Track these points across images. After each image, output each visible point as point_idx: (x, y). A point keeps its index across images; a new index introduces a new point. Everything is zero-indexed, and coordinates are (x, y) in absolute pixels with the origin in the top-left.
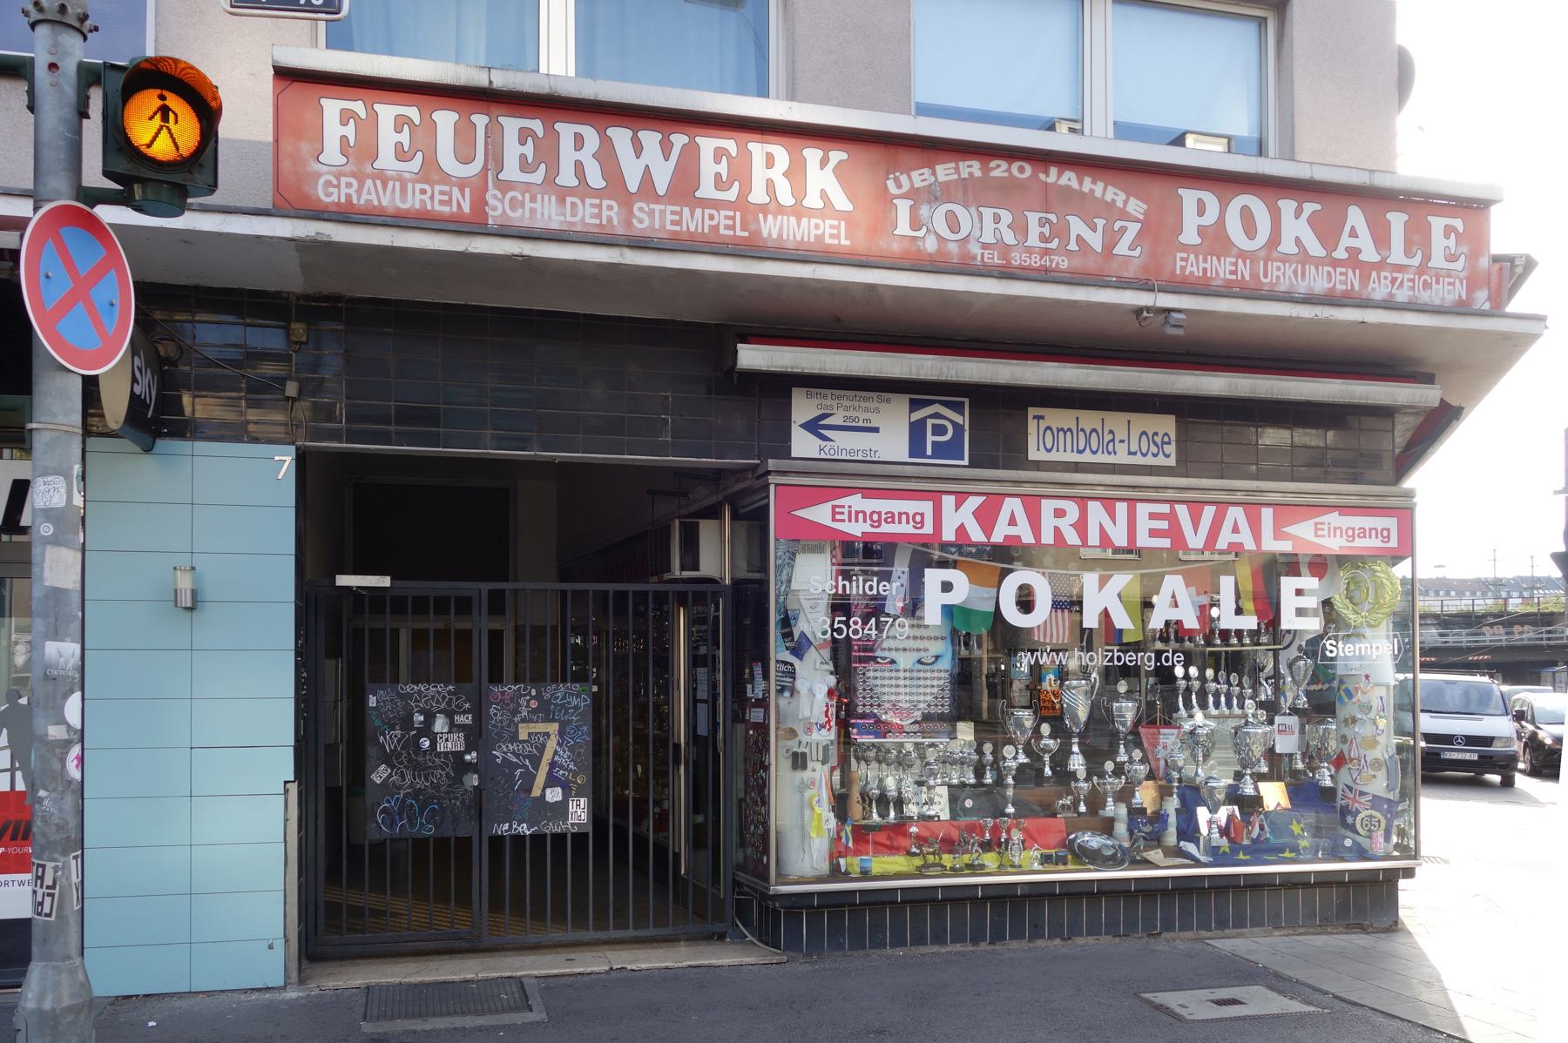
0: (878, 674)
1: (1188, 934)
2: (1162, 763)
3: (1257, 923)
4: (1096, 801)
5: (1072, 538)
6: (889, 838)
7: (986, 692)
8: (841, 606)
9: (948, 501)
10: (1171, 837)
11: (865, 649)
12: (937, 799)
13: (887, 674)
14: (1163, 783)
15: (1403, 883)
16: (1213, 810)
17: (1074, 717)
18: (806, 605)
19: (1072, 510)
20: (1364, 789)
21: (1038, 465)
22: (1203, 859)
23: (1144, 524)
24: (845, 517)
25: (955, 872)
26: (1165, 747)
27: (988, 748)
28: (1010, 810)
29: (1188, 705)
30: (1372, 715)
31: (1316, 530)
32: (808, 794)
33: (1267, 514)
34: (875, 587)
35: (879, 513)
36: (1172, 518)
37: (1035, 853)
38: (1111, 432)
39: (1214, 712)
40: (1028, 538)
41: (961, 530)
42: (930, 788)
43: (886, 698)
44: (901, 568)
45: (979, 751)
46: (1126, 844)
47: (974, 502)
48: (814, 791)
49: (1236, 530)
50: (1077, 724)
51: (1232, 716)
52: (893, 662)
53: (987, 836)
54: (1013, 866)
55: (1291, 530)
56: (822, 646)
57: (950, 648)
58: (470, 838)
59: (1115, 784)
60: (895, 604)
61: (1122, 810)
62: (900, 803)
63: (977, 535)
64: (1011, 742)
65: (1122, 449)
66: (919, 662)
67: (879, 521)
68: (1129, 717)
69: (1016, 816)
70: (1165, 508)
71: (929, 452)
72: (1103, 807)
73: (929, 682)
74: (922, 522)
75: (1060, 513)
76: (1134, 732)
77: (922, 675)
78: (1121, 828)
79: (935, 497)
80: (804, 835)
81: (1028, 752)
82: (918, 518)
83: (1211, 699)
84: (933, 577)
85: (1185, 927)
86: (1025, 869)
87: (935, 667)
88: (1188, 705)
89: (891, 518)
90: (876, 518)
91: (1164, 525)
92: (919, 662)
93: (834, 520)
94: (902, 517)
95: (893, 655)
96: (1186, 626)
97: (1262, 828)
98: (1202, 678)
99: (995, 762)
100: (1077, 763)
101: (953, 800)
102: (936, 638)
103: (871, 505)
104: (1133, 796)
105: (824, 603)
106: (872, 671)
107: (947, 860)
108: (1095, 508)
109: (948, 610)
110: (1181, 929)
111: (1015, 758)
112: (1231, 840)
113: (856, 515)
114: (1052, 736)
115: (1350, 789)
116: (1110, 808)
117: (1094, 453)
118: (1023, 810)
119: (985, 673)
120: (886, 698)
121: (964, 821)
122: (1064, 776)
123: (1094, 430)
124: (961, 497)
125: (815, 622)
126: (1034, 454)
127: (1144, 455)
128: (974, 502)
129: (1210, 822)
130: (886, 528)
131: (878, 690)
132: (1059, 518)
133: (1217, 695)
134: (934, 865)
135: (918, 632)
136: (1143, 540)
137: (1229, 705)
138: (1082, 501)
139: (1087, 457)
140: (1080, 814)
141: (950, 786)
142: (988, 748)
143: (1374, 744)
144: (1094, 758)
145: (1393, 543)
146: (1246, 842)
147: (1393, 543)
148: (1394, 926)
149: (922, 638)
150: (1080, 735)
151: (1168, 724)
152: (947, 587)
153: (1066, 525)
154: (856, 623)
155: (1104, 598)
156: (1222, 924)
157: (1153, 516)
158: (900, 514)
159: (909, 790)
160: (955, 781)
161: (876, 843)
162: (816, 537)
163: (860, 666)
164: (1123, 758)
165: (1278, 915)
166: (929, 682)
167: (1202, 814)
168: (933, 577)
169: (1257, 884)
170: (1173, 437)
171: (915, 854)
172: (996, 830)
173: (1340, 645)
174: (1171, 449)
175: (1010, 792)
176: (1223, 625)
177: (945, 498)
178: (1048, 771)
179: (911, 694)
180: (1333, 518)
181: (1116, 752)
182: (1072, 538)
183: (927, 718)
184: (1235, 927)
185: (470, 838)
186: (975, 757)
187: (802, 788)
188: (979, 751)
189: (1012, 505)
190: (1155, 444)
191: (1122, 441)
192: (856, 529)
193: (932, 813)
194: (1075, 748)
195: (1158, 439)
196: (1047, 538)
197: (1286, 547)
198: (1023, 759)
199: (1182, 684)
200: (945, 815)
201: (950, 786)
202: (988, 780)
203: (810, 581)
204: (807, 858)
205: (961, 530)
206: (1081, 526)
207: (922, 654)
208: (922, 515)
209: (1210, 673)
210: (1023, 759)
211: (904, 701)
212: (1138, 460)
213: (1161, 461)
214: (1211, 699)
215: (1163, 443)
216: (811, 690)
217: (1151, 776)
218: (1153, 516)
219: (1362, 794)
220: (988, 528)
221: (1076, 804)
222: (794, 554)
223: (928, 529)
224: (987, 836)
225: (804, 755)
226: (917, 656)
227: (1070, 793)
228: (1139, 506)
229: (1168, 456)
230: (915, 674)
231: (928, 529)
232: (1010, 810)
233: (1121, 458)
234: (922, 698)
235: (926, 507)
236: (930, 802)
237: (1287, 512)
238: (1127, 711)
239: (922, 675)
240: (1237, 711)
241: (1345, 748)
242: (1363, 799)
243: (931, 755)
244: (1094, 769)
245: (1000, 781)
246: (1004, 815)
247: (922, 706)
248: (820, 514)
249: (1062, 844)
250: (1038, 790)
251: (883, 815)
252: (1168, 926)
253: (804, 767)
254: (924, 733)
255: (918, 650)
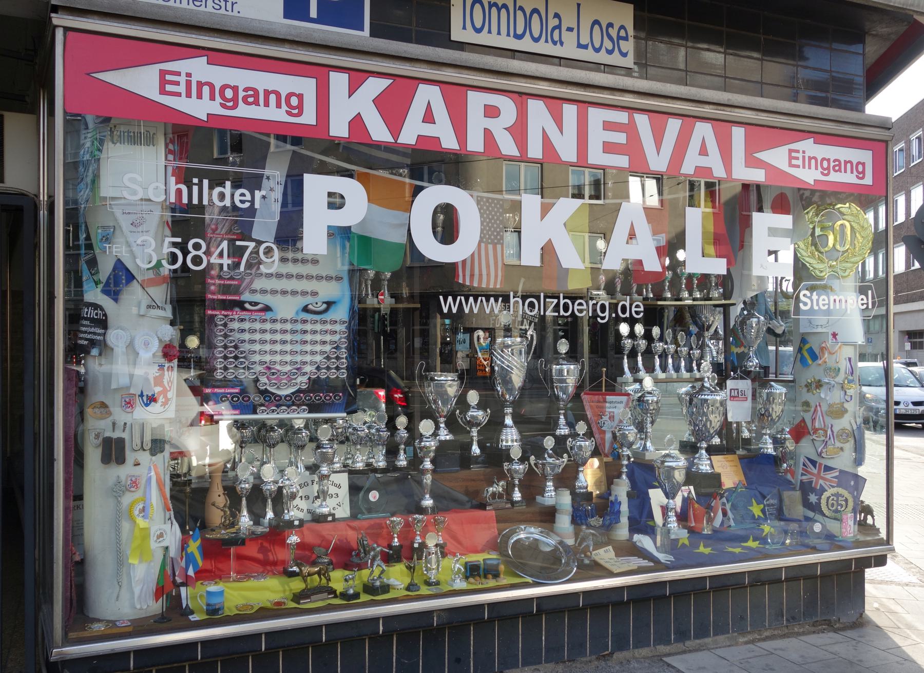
0: (246, 325)
1: (645, 652)
2: (608, 436)
3: (721, 630)
4: (532, 485)
5: (508, 146)
6: (262, 549)
7: (439, 359)
8: (185, 223)
9: (339, 82)
10: (622, 531)
11: (226, 289)
12: (332, 490)
13: (257, 326)
14: (610, 459)
15: (870, 573)
16: (670, 495)
17: (507, 382)
18: (124, 222)
19: (507, 106)
20: (830, 463)
21: (461, 46)
22: (662, 557)
23: (597, 136)
24: (182, 89)
25: (349, 599)
26: (612, 418)
27: (402, 421)
28: (428, 502)
29: (634, 369)
30: (840, 378)
31: (791, 158)
32: (127, 499)
33: (738, 133)
34: (241, 197)
35: (235, 89)
36: (630, 129)
37: (455, 564)
38: (557, 16)
39: (662, 376)
40: (449, 142)
41: (357, 123)
42: (323, 477)
43: (257, 358)
44: (275, 175)
45: (391, 425)
46: (570, 542)
47: (374, 86)
48: (138, 494)
49: (703, 151)
50: (510, 391)
51: (681, 380)
52: (267, 309)
53: (396, 542)
54: (428, 583)
55: (764, 156)
56: (153, 282)
57: (347, 294)
58: (895, 304)
59: (556, 463)
60: (265, 226)
61: (566, 499)
62: (280, 499)
63: (379, 131)
64: (430, 415)
65: (570, 39)
66: (306, 309)
67: (235, 99)
68: (571, 382)
69: (435, 510)
70: (622, 117)
71: (313, 13)
72: (542, 492)
73: (318, 337)
74: (300, 107)
75: (491, 112)
76: (577, 397)
77: (308, 327)
78: (564, 522)
79: (320, 73)
80: (121, 561)
81: (452, 424)
82: (294, 101)
83: (657, 362)
84: (316, 187)
85: (641, 643)
86: (445, 588)
87: (328, 316)
88: (634, 369)
89: (253, 96)
90: (231, 96)
91: (620, 138)
92: (306, 309)
93: (163, 91)
94: (271, 97)
95: (267, 300)
96: (647, 268)
97: (725, 514)
98: (648, 336)
99: (409, 442)
100: (510, 438)
101: (354, 489)
102: (329, 278)
103: (222, 75)
104: (576, 478)
105: (156, 217)
106: (239, 326)
107: (338, 579)
108: (536, 108)
109: (339, 234)
110: (636, 646)
111: (435, 434)
112: (691, 531)
113: (200, 89)
114: (481, 406)
115: (814, 463)
116: (551, 495)
117: (536, 40)
118: (445, 503)
119: (403, 325)
120: (257, 358)
121: (366, 520)
122: (496, 457)
123: (535, 11)
124: (357, 78)
125: (144, 246)
126: (457, 34)
127: (597, 50)
128: (374, 86)
129: (665, 510)
130: (244, 111)
131: (246, 347)
132: (487, 121)
133: (664, 356)
134: (319, 590)
135: (291, 268)
136: (596, 156)
137: (677, 369)
138: (520, 97)
139: (526, 45)
140: (513, 503)
141: (352, 473)
142: (402, 421)
143: (840, 412)
144: (535, 427)
145: (868, 180)
146: (707, 532)
147: (868, 180)
148: (860, 623)
149: (309, 277)
150: (514, 404)
151: (612, 389)
152: (336, 202)
153: (500, 128)
154: (197, 247)
155: (549, 231)
156: (683, 635)
157: (608, 126)
158: (267, 93)
159: (295, 477)
160: (360, 466)
161: (240, 557)
162: (131, 119)
163: (219, 315)
164: (563, 431)
165: (743, 618)
166: (318, 337)
167: (656, 497)
168: (316, 187)
169: (722, 584)
170: (631, 32)
171: (293, 574)
172: (408, 532)
173: (815, 297)
174: (628, 46)
175: (428, 479)
176: (689, 269)
177: (333, 75)
178: (476, 450)
179: (293, 353)
180: (808, 146)
181: (556, 425)
182: (508, 146)
183: (316, 385)
184: (697, 637)
185: (895, 304)
186: (385, 434)
187: (118, 490)
188: (391, 425)
189: (428, 95)
190: (610, 38)
191: (570, 29)
192: (200, 109)
193: (325, 510)
194: (508, 421)
195: (613, 32)
196: (475, 144)
197: (757, 176)
198: (445, 435)
199: (628, 343)
200: (344, 512)
201: (352, 473)
202: (402, 462)
203: (136, 181)
204: (125, 595)
205: (357, 123)
206: (519, 131)
207: (308, 300)
208: (300, 97)
209: (656, 331)
210: (445, 435)
211: (283, 363)
212: (588, 55)
213: (615, 59)
214: (657, 362)
215: (620, 38)
216: (131, 346)
217: (596, 453)
218: (608, 126)
219: (828, 469)
220: (395, 123)
221: (509, 491)
222: (101, 142)
223: (309, 117)
224: (396, 542)
225: (121, 442)
226: (301, 301)
227: (501, 476)
228: (592, 111)
229: (624, 55)
230: (299, 327)
231: (309, 117)
232: (428, 502)
233: (569, 50)
234: (308, 358)
235: (307, 86)
236: (323, 495)
237: (764, 134)
238: (568, 374)
239: (308, 327)
240: (685, 374)
241: (808, 418)
242: (829, 475)
243: (324, 433)
244: (531, 448)
245: (415, 461)
246: (421, 510)
247: (308, 369)
248: (142, 81)
249: (497, 546)
250: (464, 473)
251: (257, 517)
252: (621, 644)
253: (121, 460)
254: (313, 408)
255: (304, 293)
